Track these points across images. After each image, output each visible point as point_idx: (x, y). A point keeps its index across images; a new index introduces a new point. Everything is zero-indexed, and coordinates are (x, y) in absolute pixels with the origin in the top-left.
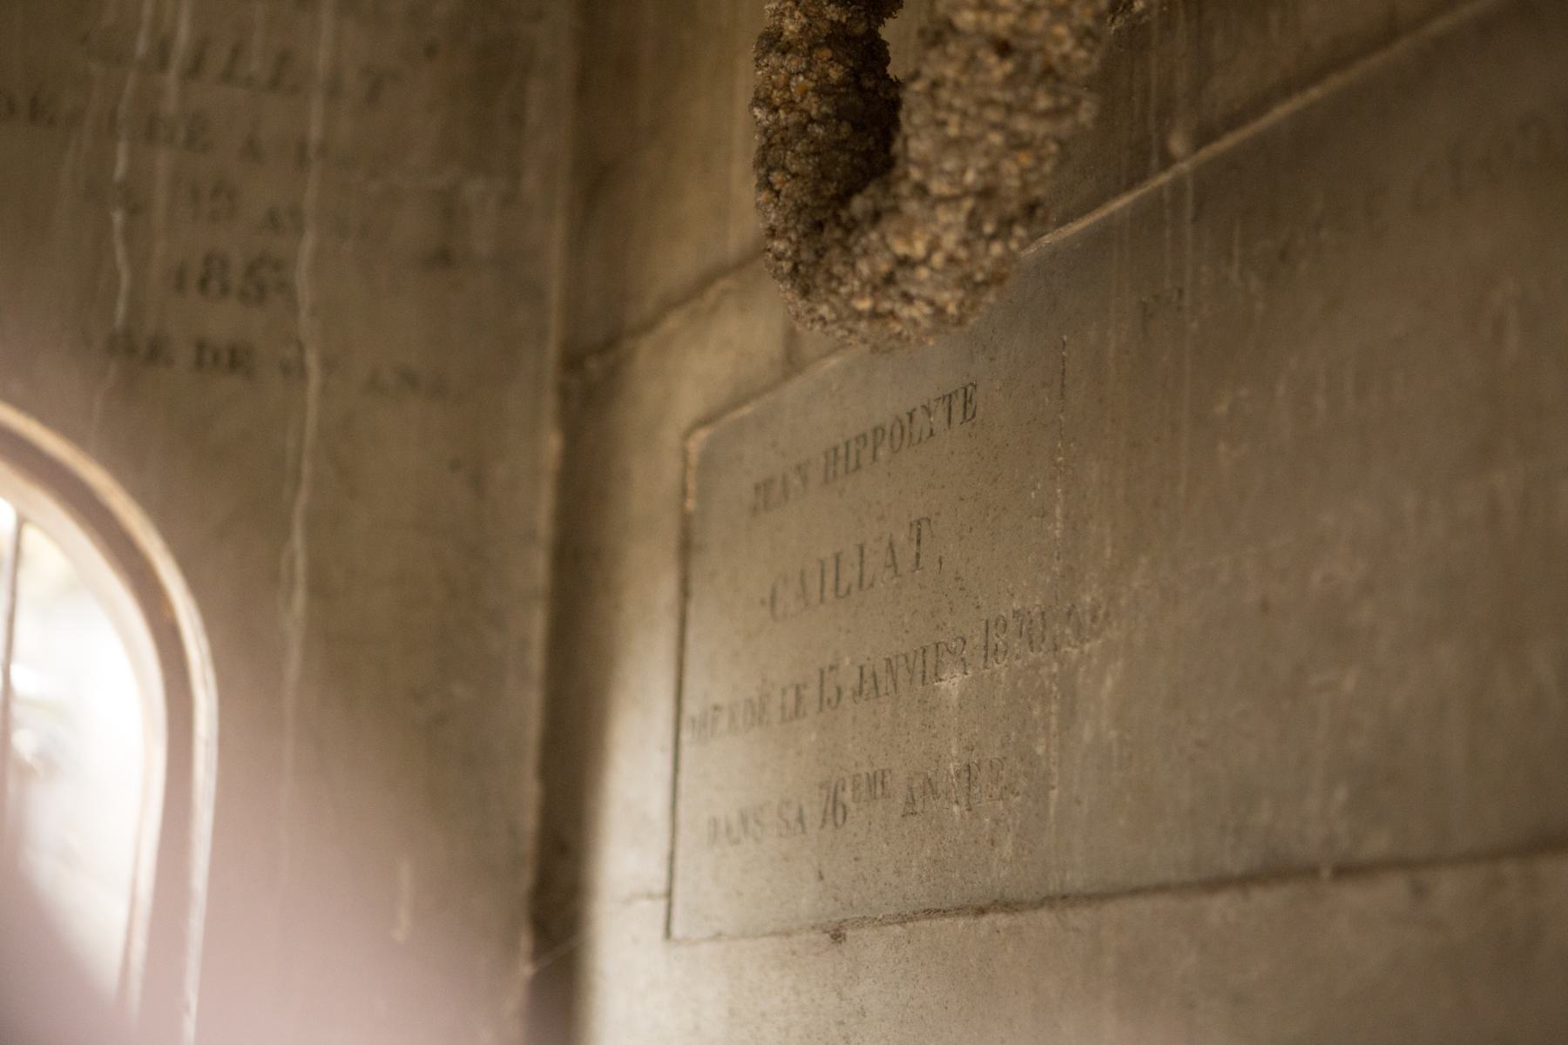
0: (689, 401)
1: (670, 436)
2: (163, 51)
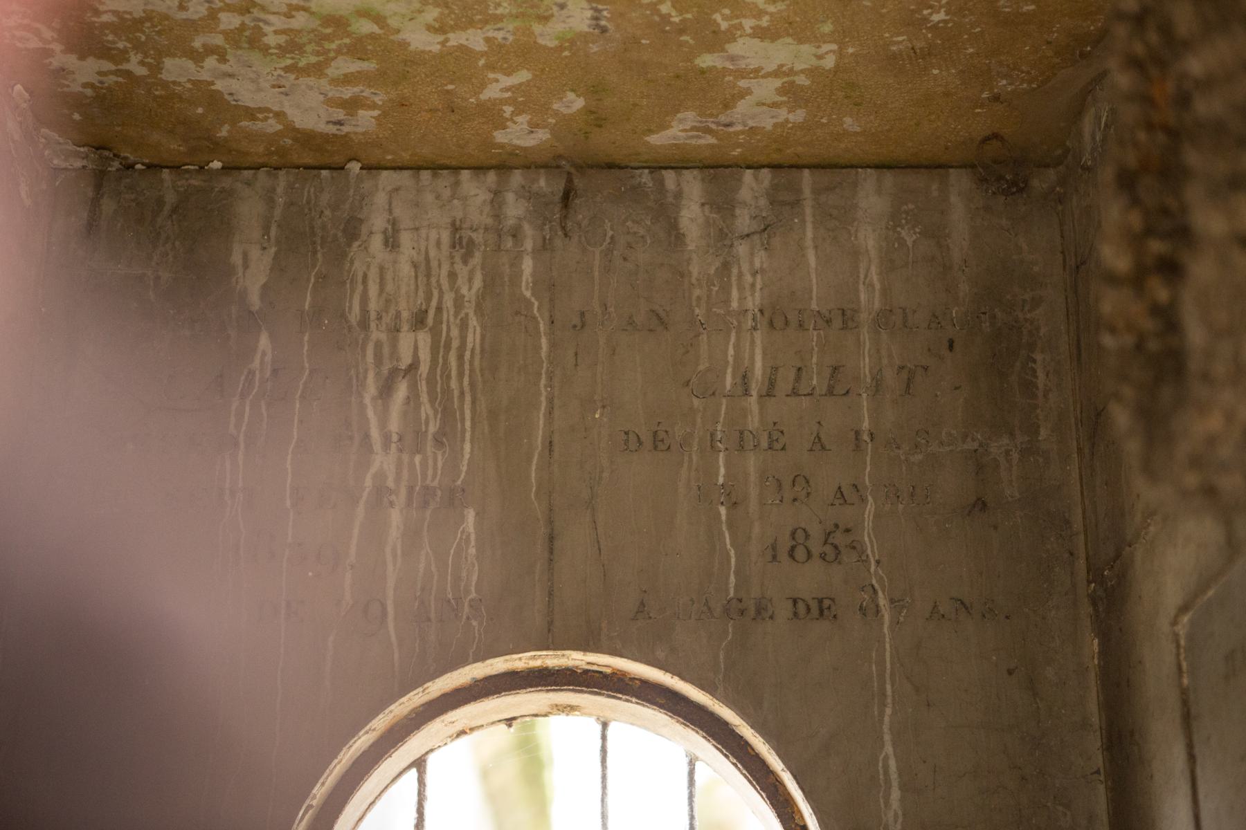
0: (1172, 591)
1: (1163, 624)
2: (745, 379)
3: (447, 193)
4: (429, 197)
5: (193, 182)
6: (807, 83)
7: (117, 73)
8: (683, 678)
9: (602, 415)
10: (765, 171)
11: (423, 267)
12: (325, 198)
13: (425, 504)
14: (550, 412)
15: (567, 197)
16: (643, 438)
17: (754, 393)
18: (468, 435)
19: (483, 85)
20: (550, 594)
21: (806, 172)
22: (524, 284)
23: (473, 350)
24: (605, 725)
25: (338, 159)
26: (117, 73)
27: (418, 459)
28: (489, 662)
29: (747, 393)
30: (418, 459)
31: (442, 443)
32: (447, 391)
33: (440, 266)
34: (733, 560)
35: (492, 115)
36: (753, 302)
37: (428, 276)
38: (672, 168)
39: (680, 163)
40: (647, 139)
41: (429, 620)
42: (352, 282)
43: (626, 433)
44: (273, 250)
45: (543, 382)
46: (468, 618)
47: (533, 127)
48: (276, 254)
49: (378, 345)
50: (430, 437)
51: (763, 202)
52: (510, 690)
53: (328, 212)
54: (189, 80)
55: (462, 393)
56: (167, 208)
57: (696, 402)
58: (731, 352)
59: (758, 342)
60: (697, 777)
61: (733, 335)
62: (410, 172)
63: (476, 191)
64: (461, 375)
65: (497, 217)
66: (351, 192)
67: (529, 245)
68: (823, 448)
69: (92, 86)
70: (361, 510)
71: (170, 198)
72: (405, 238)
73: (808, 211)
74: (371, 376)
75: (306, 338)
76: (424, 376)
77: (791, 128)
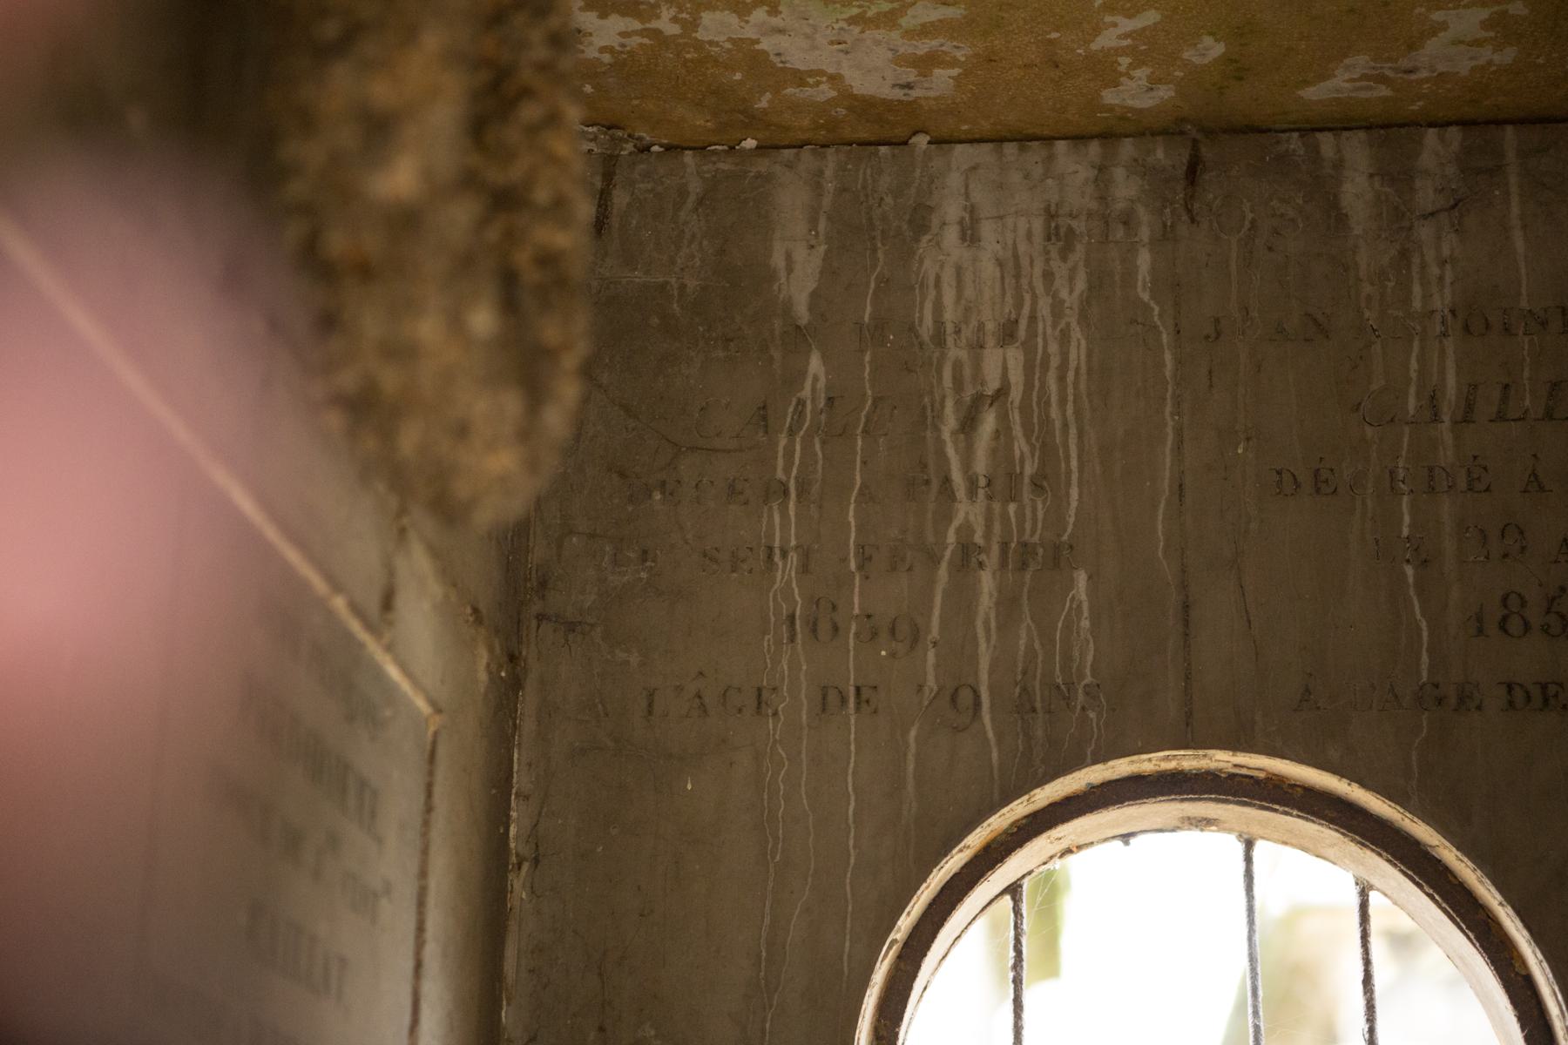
2: (1433, 402)
3: (1038, 171)
4: (1016, 177)
5: (722, 166)
6: (1525, 12)
7: (641, 33)
8: (1363, 785)
9: (1246, 450)
10: (1453, 130)
11: (1011, 264)
12: (885, 181)
13: (1024, 566)
14: (1179, 447)
15: (1193, 171)
16: (1300, 479)
17: (1446, 418)
18: (1075, 477)
19: (1097, 31)
20: (1187, 678)
21: (1509, 129)
22: (1140, 284)
23: (1077, 370)
24: (1249, 845)
25: (900, 132)
26: (641, 33)
27: (1012, 508)
28: (1111, 763)
29: (1436, 418)
30: (1012, 508)
31: (1042, 487)
32: (1046, 421)
33: (1032, 262)
34: (1425, 634)
35: (1104, 70)
36: (1442, 301)
37: (1017, 276)
38: (1330, 129)
39: (1342, 123)
40: (1300, 93)
41: (1034, 710)
42: (922, 286)
43: (1279, 473)
44: (823, 248)
45: (1168, 409)
46: (1083, 708)
47: (1154, 82)
48: (827, 252)
49: (958, 366)
50: (1027, 480)
51: (1451, 170)
52: (1135, 799)
53: (889, 200)
54: (730, 39)
55: (1065, 425)
56: (692, 199)
57: (1369, 431)
58: (1414, 365)
59: (1450, 351)
60: (1372, 911)
61: (1416, 344)
62: (990, 146)
63: (1074, 167)
64: (1063, 401)
65: (1102, 199)
66: (918, 172)
67: (1145, 233)
68: (1541, 488)
69: (610, 50)
70: (943, 571)
71: (695, 187)
72: (987, 230)
73: (1513, 180)
74: (949, 405)
75: (867, 358)
76: (1017, 403)
77: (1494, 72)
